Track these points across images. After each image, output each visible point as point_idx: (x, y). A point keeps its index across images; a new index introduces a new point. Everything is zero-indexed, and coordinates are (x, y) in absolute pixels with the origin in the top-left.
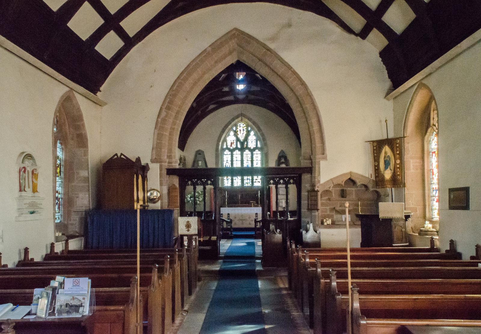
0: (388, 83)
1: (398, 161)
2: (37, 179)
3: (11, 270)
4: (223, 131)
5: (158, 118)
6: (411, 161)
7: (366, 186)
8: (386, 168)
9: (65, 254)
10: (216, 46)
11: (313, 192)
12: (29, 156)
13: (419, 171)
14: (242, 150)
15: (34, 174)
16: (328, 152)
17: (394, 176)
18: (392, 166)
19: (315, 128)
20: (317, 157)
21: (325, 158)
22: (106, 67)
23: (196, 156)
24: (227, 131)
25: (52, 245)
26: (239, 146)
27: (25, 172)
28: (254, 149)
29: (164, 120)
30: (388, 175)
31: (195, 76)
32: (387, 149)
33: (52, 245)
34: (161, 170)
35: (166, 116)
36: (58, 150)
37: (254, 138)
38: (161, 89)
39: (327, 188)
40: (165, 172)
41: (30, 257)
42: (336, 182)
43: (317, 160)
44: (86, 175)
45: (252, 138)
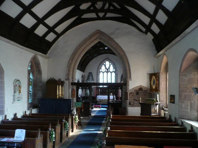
0: (156, 52)
1: (158, 82)
2: (20, 88)
3: (19, 118)
4: (100, 65)
5: (68, 63)
6: (163, 82)
7: (147, 91)
8: (153, 84)
9: (31, 115)
10: (91, 37)
11: (126, 93)
12: (18, 80)
13: (165, 86)
14: (107, 72)
15: (20, 87)
16: (132, 78)
17: (156, 87)
18: (156, 83)
19: (128, 68)
20: (128, 79)
21: (131, 80)
22: (49, 45)
23: (89, 74)
24: (101, 64)
25: (25, 112)
26: (106, 71)
27: (16, 86)
28: (112, 72)
29: (71, 64)
30: (154, 87)
31: (83, 48)
32: (154, 77)
33: (25, 112)
34: (69, 83)
35: (71, 63)
36: (31, 76)
37: (113, 67)
38: (70, 52)
39: (131, 91)
40: (70, 84)
41: (7, 118)
42: (135, 89)
43: (128, 81)
44: (41, 85)
45: (112, 67)
